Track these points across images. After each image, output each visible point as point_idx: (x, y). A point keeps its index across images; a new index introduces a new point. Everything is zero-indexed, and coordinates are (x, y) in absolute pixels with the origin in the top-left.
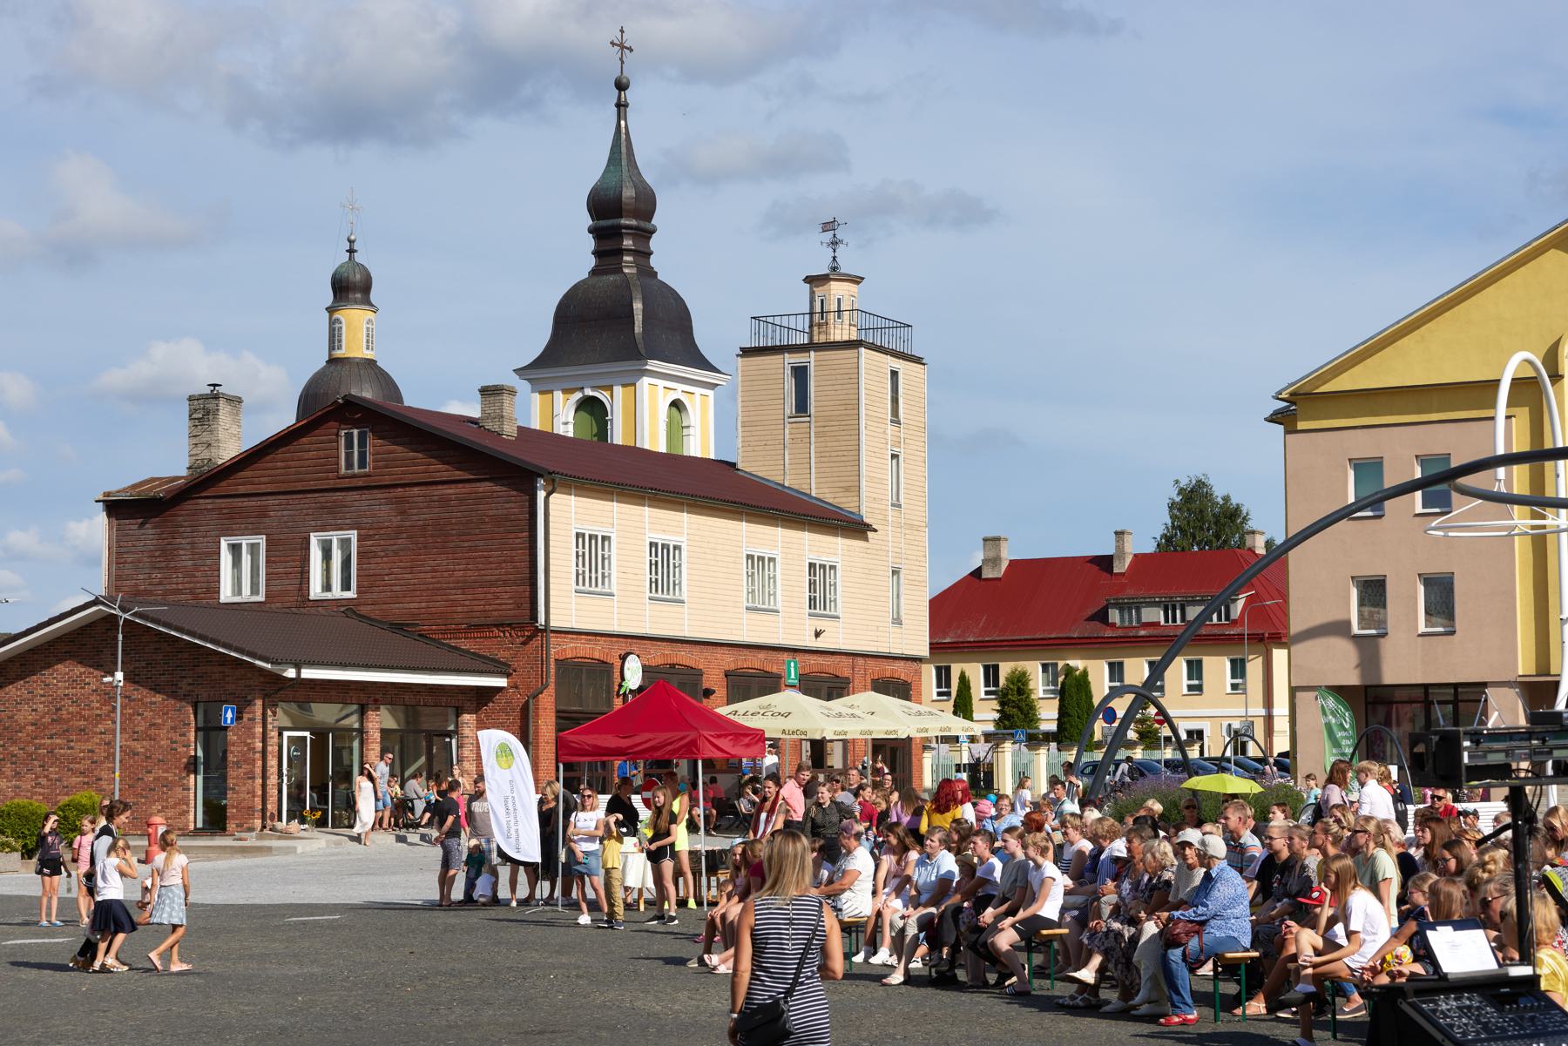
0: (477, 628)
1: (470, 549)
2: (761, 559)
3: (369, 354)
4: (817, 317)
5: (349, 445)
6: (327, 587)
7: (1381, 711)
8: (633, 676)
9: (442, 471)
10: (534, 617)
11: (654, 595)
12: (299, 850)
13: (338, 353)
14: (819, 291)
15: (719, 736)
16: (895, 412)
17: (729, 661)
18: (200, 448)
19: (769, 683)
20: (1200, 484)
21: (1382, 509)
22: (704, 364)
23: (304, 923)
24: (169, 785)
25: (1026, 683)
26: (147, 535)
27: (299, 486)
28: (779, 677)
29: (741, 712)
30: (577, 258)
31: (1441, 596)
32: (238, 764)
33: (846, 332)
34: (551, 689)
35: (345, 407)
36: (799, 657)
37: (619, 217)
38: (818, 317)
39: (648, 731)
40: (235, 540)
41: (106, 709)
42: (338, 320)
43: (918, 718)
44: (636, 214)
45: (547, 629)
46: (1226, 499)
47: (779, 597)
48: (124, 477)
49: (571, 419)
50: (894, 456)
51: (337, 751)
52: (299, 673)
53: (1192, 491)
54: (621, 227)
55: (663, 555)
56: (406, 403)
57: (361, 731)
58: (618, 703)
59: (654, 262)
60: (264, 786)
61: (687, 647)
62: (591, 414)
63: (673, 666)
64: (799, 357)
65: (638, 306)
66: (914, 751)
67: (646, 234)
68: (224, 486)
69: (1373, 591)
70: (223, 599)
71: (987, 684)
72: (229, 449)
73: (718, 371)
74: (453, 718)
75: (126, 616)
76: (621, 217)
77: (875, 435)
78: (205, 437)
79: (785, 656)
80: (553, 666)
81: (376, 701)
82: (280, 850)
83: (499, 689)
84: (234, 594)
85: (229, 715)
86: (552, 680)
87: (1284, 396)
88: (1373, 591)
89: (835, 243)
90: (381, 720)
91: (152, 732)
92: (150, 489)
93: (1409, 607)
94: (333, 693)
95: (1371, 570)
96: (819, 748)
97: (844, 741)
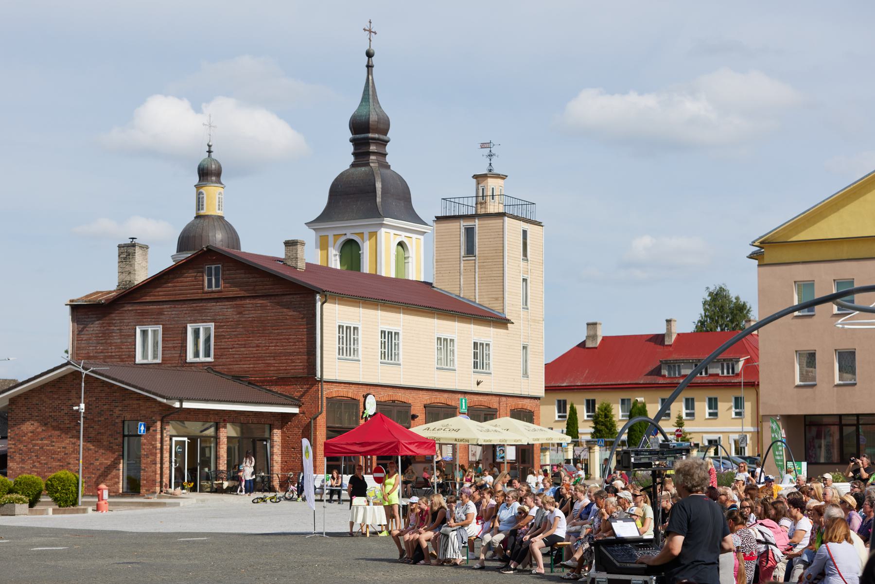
3: (219, 213)
7: (814, 430)
8: (371, 407)
11: (383, 361)
12: (181, 505)
13: (202, 212)
15: (410, 444)
17: (427, 398)
19: (450, 412)
20: (721, 289)
21: (813, 311)
22: (417, 220)
23: (188, 541)
25: (610, 411)
27: (181, 298)
28: (456, 408)
29: (432, 428)
30: (342, 158)
31: (847, 361)
32: (147, 456)
33: (496, 207)
34: (324, 413)
36: (468, 397)
37: (368, 134)
38: (481, 199)
39: (375, 441)
40: (144, 328)
41: (73, 424)
43: (546, 432)
45: (321, 380)
46: (737, 298)
48: (81, 292)
51: (203, 450)
52: (181, 405)
53: (717, 294)
55: (389, 337)
56: (242, 250)
57: (217, 438)
58: (362, 422)
60: (161, 468)
61: (402, 391)
63: (394, 401)
64: (471, 226)
65: (379, 185)
69: (810, 359)
72: (141, 276)
73: (426, 224)
75: (87, 372)
76: (369, 132)
77: (514, 267)
78: (128, 268)
79: (460, 396)
82: (171, 505)
83: (294, 414)
85: (142, 428)
86: (324, 409)
87: (757, 243)
88: (810, 359)
89: (490, 155)
90: (229, 431)
91: (99, 437)
93: (830, 371)
94: (200, 416)
95: (810, 347)
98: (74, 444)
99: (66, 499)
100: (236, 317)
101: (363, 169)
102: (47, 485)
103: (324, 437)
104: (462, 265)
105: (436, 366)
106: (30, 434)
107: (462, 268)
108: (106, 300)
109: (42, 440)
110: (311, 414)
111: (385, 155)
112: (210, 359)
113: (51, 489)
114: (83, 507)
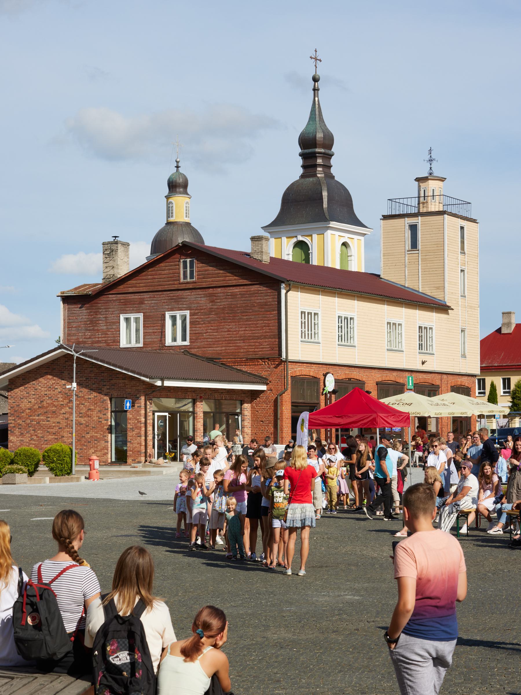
0: (251, 360)
1: (247, 320)
2: (394, 324)
3: (187, 220)
4: (422, 199)
5: (185, 267)
6: (174, 339)
8: (330, 385)
9: (233, 279)
10: (280, 355)
12: (164, 473)
13: (171, 220)
14: (423, 185)
16: (463, 248)
17: (379, 377)
18: (108, 269)
19: (398, 389)
22: (359, 223)
24: (97, 440)
26: (82, 313)
28: (403, 385)
30: (293, 170)
32: (132, 429)
34: (289, 391)
35: (177, 249)
36: (414, 375)
37: (315, 148)
40: (127, 316)
42: (171, 203)
44: (324, 146)
45: (286, 361)
47: (404, 344)
48: (69, 286)
49: (291, 253)
50: (462, 271)
51: (182, 423)
52: (163, 383)
54: (315, 153)
55: (345, 322)
57: (193, 413)
59: (333, 171)
60: (146, 440)
62: (301, 249)
65: (325, 194)
66: (472, 423)
67: (328, 156)
68: (121, 288)
70: (122, 346)
71: (504, 388)
72: (122, 271)
73: (366, 227)
74: (239, 406)
76: (316, 148)
79: (407, 374)
80: (290, 379)
81: (201, 397)
83: (263, 391)
84: (127, 343)
85: (128, 404)
89: (431, 160)
90: (202, 407)
91: (89, 413)
92: (84, 290)
94: (180, 393)
96: (423, 421)
97: (437, 418)
98: (67, 419)
99: (61, 467)
100: (209, 305)
101: (311, 179)
102: (44, 456)
103: (289, 411)
104: (407, 258)
105: (386, 348)
106: (28, 411)
107: (407, 261)
108: (93, 291)
109: (38, 416)
110: (277, 391)
111: (330, 167)
112: (187, 343)
113: (47, 459)
114: (76, 476)
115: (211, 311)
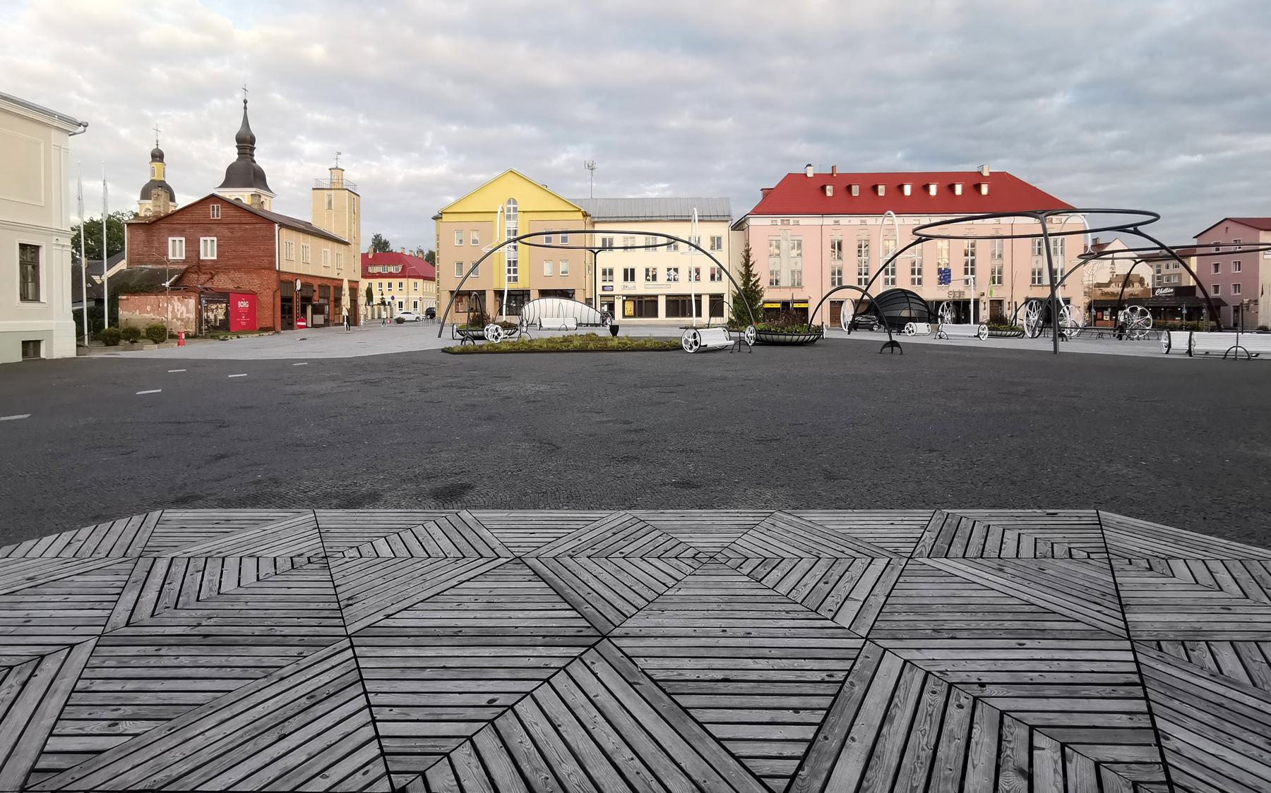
17: (319, 282)
37: (246, 143)
68: (169, 220)
115: (231, 238)
